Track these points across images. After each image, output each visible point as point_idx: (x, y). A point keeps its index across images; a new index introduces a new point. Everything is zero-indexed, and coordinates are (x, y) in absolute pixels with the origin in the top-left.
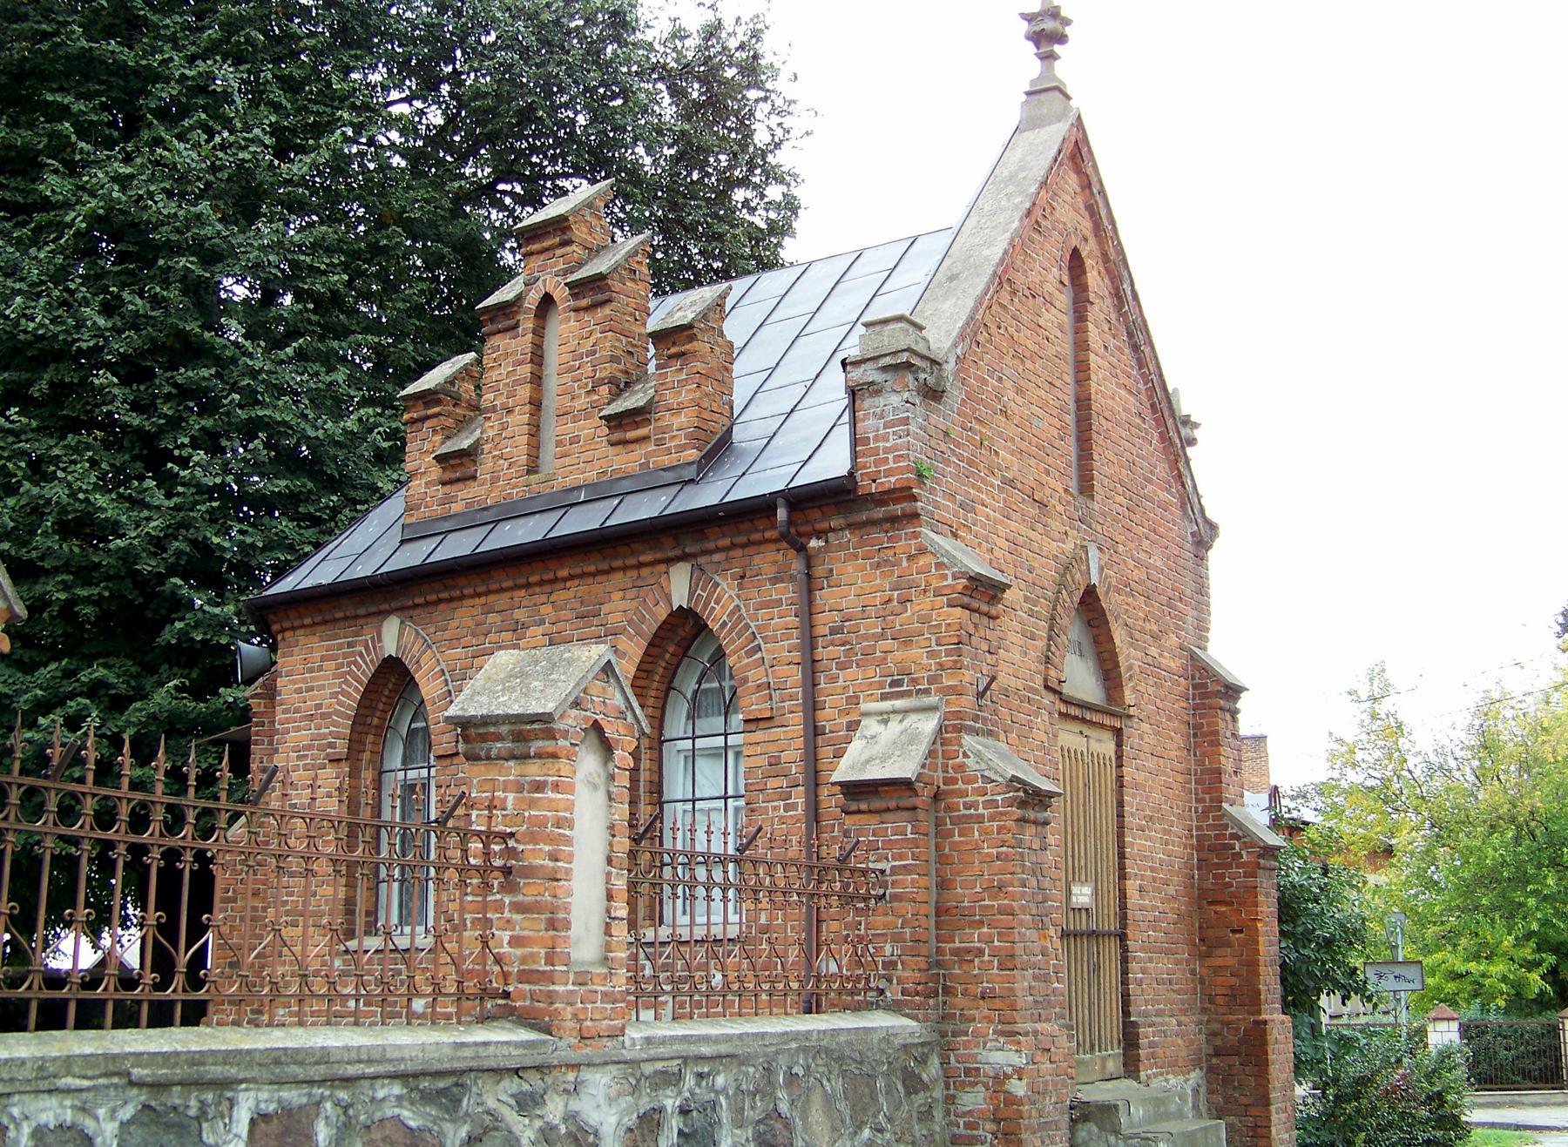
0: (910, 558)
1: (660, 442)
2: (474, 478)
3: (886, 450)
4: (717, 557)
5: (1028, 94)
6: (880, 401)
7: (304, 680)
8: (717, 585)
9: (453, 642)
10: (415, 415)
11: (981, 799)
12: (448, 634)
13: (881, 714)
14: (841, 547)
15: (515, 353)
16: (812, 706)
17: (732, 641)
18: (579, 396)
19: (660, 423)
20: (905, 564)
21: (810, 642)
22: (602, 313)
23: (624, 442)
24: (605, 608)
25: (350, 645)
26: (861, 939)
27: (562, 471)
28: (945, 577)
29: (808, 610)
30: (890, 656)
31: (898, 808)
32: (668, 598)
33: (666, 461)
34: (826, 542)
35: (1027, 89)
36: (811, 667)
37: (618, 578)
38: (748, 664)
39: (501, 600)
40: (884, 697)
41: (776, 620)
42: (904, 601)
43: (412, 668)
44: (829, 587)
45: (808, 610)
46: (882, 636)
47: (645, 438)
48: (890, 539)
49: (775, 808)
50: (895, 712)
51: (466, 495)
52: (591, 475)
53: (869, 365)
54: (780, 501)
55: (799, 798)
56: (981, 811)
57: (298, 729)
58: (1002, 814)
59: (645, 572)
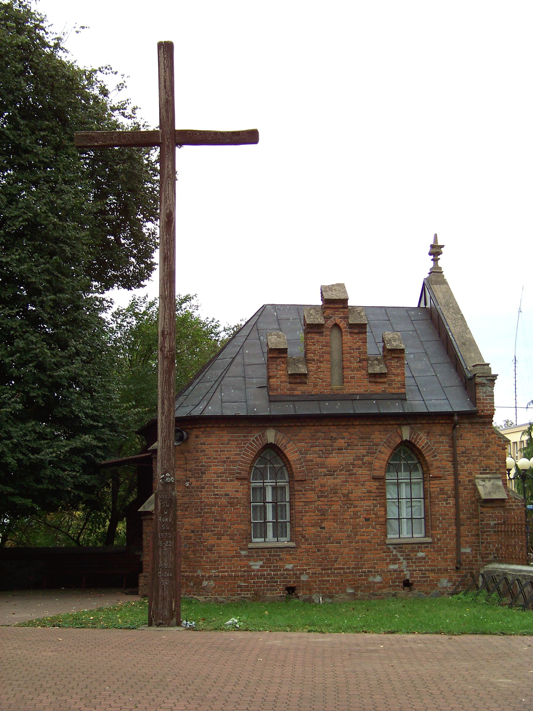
0: (489, 434)
1: (389, 385)
2: (306, 383)
3: (487, 403)
4: (418, 425)
5: (429, 273)
6: (484, 388)
7: (219, 447)
8: (419, 434)
9: (300, 441)
10: (275, 356)
11: (514, 504)
12: (297, 438)
13: (482, 478)
14: (465, 428)
15: (323, 342)
16: (456, 474)
17: (427, 452)
18: (354, 363)
19: (389, 378)
20: (487, 436)
21: (454, 455)
22: (361, 336)
23: (376, 382)
24: (373, 436)
25: (244, 436)
26: (488, 543)
27: (350, 389)
28: (501, 441)
29: (453, 446)
30: (482, 462)
31: (500, 507)
32: (401, 437)
33: (393, 391)
34: (460, 426)
35: (429, 272)
36: (455, 463)
37: (378, 427)
38: (433, 460)
39: (325, 429)
40: (481, 474)
41: (442, 447)
42: (488, 447)
43: (282, 449)
44: (461, 439)
45: (453, 446)
46: (480, 456)
47: (384, 383)
48: (482, 428)
49: (442, 504)
50: (487, 478)
51: (300, 390)
52: (362, 391)
53: (483, 378)
54: (456, 414)
55: (452, 501)
56: (514, 507)
57: (217, 466)
58: (521, 508)
59: (389, 427)
